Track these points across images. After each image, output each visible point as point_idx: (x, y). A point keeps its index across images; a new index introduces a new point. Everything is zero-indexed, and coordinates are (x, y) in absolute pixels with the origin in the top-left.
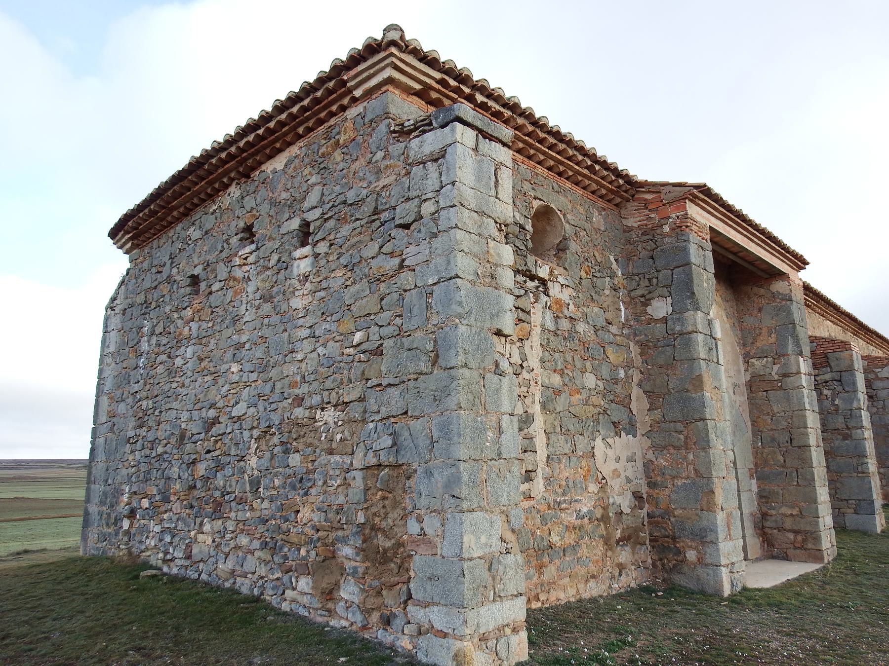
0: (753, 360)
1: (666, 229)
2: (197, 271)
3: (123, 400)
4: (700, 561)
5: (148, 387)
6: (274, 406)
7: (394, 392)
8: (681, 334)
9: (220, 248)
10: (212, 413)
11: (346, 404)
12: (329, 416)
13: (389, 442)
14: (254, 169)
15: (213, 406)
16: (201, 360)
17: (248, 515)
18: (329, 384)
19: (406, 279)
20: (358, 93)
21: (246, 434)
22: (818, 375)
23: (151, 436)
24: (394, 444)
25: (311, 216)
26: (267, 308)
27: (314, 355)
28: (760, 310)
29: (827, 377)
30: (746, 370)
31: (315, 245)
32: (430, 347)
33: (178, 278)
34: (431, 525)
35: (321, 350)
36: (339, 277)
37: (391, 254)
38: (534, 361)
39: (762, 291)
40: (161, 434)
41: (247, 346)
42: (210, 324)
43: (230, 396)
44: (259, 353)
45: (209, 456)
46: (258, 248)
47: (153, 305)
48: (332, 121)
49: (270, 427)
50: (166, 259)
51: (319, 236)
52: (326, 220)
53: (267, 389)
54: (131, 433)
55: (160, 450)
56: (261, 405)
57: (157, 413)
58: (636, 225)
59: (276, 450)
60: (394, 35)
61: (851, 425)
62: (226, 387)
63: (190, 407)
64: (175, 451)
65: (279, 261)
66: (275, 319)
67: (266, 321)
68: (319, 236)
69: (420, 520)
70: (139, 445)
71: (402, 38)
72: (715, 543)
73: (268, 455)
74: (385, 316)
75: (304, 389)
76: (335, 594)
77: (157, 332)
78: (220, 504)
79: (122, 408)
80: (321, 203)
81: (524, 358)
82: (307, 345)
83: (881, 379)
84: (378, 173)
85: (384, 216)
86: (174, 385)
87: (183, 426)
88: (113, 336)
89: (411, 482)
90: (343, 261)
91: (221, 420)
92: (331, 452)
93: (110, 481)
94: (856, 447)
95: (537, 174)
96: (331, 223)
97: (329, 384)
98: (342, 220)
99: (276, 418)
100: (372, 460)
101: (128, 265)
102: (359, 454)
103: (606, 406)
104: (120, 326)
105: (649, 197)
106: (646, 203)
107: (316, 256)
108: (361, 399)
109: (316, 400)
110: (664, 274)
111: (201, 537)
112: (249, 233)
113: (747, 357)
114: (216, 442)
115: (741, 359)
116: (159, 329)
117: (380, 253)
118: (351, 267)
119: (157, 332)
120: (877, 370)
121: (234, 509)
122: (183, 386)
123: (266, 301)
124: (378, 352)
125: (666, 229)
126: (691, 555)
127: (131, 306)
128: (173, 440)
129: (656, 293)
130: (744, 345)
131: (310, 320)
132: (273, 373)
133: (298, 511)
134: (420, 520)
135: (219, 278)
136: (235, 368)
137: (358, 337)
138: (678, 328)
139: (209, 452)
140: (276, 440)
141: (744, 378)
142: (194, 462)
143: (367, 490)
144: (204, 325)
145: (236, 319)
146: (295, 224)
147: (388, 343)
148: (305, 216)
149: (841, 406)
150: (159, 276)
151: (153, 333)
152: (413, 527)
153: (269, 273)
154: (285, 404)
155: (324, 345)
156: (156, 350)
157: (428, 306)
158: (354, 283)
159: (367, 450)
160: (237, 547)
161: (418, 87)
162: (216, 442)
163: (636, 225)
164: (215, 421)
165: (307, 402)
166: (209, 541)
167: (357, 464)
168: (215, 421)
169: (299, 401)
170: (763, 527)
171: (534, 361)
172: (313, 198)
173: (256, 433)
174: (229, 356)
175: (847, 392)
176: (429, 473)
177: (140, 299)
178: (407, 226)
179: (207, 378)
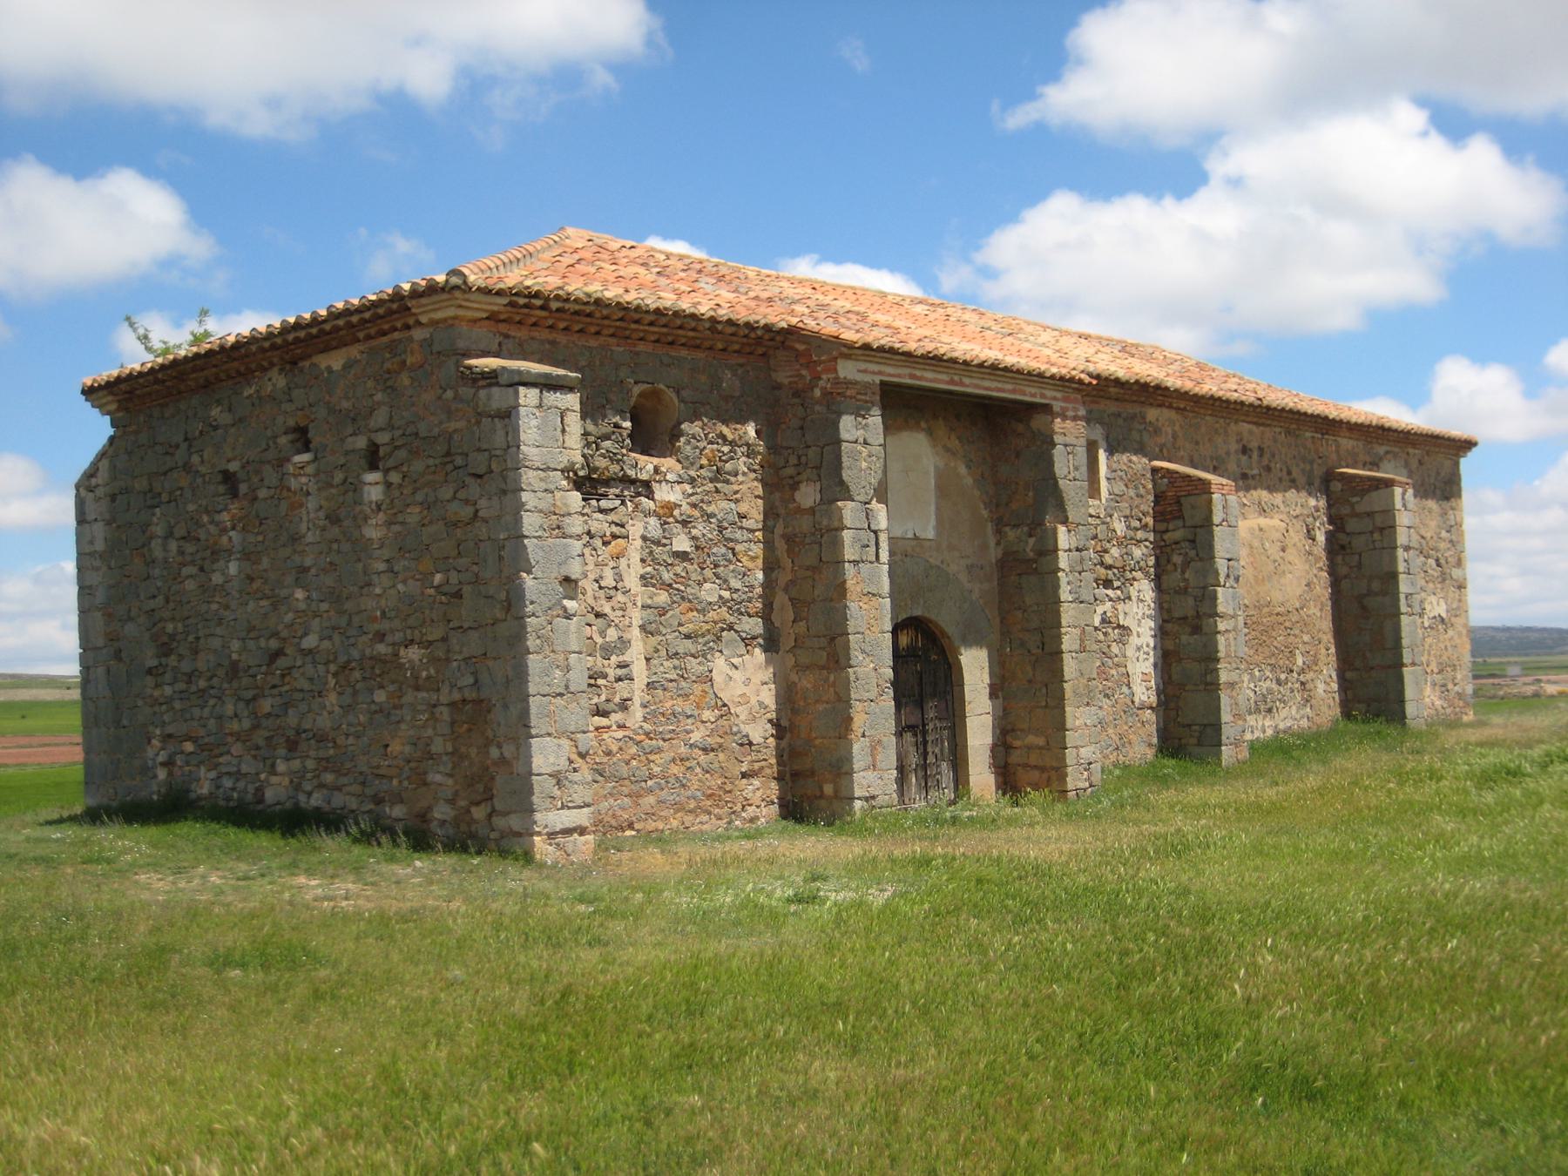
0: (1007, 529)
1: (817, 393)
2: (233, 467)
3: (130, 619)
4: (837, 795)
5: (172, 605)
6: (352, 640)
7: (474, 635)
8: (829, 530)
9: (264, 446)
10: (274, 644)
11: (431, 643)
12: (413, 654)
13: (471, 680)
14: (302, 359)
15: (275, 634)
16: (251, 579)
17: (331, 752)
18: (411, 621)
19: (482, 530)
20: (424, 319)
21: (321, 668)
22: (1167, 531)
23: (186, 667)
24: (476, 681)
25: (382, 438)
26: (335, 531)
27: (392, 591)
28: (1018, 455)
29: (1178, 535)
30: (998, 544)
31: (386, 471)
32: (503, 596)
33: (203, 469)
34: (508, 750)
35: (400, 587)
36: (414, 515)
37: (467, 502)
38: (632, 581)
39: (1020, 428)
40: (201, 665)
41: (313, 571)
42: (260, 538)
43: (297, 627)
44: (329, 580)
45: (275, 691)
46: (316, 459)
47: (165, 497)
48: (396, 335)
49: (349, 662)
50: (179, 438)
51: (391, 463)
52: (396, 448)
53: (343, 621)
54: (155, 663)
55: (202, 684)
56: (337, 638)
57: (191, 638)
58: (786, 381)
59: (359, 686)
60: (455, 280)
61: (1202, 610)
62: (290, 616)
63: (243, 634)
64: (225, 685)
65: (345, 481)
66: (346, 547)
67: (335, 546)
68: (391, 463)
69: (499, 746)
70: (168, 677)
71: (465, 282)
72: (850, 773)
73: (349, 690)
74: (463, 561)
75: (385, 625)
76: (429, 816)
77: (177, 535)
78: (296, 743)
79: (130, 629)
80: (390, 427)
81: (619, 577)
82: (386, 580)
83: (1357, 515)
84: (450, 413)
85: (459, 461)
86: (214, 607)
87: (235, 656)
88: (99, 530)
89: (491, 716)
90: (419, 497)
91: (288, 651)
92: (417, 688)
93: (125, 722)
94: (1205, 646)
95: (637, 354)
96: (402, 454)
97: (411, 621)
98: (415, 453)
99: (355, 654)
100: (457, 696)
101: (111, 431)
102: (445, 689)
103: (732, 619)
104: (107, 516)
105: (800, 347)
106: (798, 354)
107: (388, 485)
108: (444, 639)
109: (398, 637)
110: (812, 453)
111: (274, 779)
112: (302, 438)
113: (999, 525)
114: (283, 676)
115: (989, 528)
116: (180, 531)
117: (454, 498)
118: (427, 506)
119: (177, 535)
120: (1355, 499)
121: (1137, 501)
122: (227, 607)
123: (332, 523)
124: (458, 595)
125: (817, 393)
126: (828, 789)
127: (126, 491)
128: (221, 672)
129: (804, 476)
130: (997, 506)
131: (386, 553)
132: (348, 606)
133: (387, 746)
134: (499, 746)
135: (266, 482)
136: (300, 594)
137: (438, 578)
138: (825, 522)
139: (274, 687)
140: (357, 675)
141: (994, 553)
142: (254, 698)
143: (453, 723)
144: (252, 539)
145: (295, 539)
146: (361, 442)
147: (467, 589)
148: (373, 436)
149: (1192, 583)
150: (168, 458)
151: (170, 534)
152: (494, 752)
153: (333, 491)
154: (365, 638)
155: (404, 582)
156: (180, 559)
157: (501, 558)
158: (431, 522)
159: (453, 686)
160: (321, 786)
161: (485, 315)
162: (283, 676)
163: (786, 381)
164: (278, 653)
165: (389, 639)
166: (286, 781)
167: (444, 699)
168: (278, 653)
169: (380, 637)
170: (1006, 765)
171: (632, 581)
172: (380, 418)
173: (333, 668)
174: (289, 579)
175: (1201, 560)
176: (506, 707)
177: (140, 485)
178: (480, 477)
179: (262, 603)
